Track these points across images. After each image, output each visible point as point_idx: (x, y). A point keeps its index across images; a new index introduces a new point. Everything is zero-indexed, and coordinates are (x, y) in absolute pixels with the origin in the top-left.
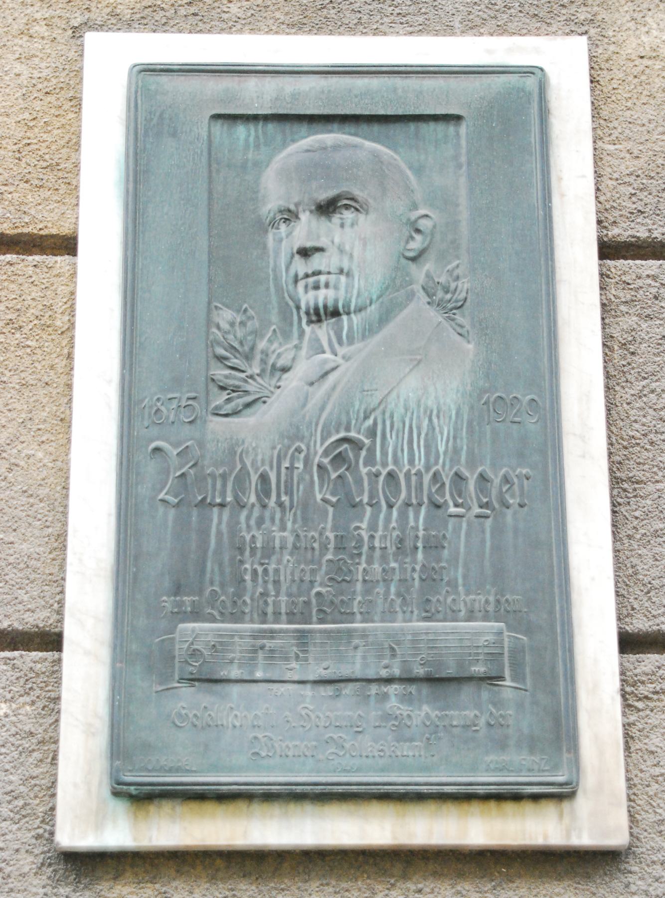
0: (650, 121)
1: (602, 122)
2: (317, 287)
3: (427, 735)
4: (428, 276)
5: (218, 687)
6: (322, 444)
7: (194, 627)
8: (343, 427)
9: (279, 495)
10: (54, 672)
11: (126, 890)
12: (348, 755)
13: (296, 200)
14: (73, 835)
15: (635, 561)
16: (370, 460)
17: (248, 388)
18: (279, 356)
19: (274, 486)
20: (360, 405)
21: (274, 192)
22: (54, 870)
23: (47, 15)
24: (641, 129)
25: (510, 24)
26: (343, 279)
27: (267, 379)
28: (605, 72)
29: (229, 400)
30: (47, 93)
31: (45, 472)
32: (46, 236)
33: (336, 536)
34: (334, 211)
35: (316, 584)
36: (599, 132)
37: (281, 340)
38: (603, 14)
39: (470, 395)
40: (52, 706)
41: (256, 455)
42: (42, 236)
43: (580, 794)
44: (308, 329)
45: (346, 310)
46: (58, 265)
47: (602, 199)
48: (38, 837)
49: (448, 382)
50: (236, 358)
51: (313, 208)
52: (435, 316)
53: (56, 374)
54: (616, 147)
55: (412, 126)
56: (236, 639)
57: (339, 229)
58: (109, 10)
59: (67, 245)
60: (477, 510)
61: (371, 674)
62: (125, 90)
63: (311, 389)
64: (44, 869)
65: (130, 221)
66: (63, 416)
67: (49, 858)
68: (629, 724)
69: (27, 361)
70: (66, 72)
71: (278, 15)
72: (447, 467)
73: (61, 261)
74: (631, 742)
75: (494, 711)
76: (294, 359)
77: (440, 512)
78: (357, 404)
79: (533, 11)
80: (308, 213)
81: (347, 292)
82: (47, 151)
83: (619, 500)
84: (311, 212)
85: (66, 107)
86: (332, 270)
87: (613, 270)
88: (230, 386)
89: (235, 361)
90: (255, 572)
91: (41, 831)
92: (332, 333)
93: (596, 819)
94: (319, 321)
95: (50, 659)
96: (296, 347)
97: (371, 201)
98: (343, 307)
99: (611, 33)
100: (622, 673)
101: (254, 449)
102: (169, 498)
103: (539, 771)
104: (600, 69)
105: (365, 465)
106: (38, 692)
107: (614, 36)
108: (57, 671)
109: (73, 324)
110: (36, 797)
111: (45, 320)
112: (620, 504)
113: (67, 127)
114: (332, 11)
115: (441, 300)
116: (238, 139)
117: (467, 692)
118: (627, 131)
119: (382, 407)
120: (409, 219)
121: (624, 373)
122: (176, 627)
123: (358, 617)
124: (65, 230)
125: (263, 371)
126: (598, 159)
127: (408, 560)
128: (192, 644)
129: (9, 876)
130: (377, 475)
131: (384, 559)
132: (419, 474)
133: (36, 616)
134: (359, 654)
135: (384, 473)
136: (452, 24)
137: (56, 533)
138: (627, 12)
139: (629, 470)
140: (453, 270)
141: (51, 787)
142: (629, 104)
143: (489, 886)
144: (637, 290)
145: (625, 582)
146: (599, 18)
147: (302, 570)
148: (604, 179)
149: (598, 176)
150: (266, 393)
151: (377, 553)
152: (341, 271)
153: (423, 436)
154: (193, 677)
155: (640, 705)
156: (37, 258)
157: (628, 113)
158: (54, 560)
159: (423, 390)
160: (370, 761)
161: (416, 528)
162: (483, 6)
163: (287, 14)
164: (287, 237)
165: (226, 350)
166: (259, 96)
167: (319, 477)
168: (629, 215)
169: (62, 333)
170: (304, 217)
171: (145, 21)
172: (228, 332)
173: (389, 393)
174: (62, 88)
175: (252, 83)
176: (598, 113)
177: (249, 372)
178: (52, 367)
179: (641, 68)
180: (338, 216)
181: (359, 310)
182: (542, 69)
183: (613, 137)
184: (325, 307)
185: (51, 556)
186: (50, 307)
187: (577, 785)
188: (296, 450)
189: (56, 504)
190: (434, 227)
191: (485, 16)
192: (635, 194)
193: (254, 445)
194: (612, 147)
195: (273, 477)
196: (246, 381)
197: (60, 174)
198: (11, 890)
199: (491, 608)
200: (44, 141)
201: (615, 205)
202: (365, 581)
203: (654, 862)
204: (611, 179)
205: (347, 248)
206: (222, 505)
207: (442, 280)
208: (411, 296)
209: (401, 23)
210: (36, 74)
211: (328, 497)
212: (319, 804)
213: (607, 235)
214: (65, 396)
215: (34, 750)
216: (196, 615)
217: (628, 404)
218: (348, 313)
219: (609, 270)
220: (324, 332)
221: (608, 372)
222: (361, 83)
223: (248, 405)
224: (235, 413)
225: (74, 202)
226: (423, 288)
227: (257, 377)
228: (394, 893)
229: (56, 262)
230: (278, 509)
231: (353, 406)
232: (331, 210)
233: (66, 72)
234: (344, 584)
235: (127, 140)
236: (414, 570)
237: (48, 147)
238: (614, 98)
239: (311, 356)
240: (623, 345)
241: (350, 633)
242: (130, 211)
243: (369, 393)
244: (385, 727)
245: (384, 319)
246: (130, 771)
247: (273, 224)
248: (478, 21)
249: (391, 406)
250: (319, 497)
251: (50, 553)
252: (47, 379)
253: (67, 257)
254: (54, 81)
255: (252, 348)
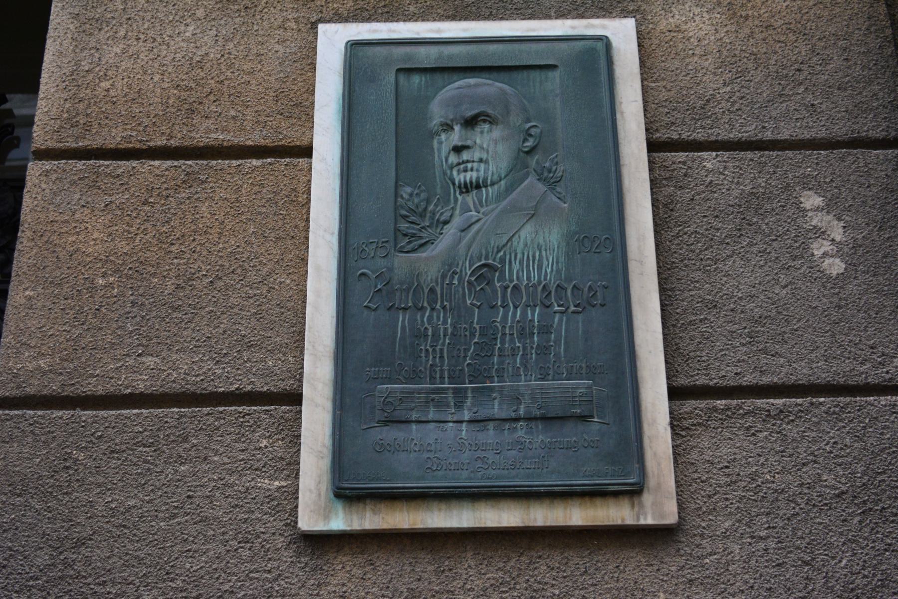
0: (677, 69)
2: (466, 171)
4: (537, 162)
9: (442, 302)
10: (297, 419)
13: (451, 117)
14: (307, 522)
15: (677, 341)
16: (502, 278)
17: (422, 235)
18: (442, 214)
19: (439, 296)
21: (437, 112)
26: (482, 165)
34: (476, 124)
38: (644, 7)
43: (645, 490)
44: (460, 198)
47: (648, 115)
48: (287, 525)
52: (541, 187)
57: (479, 135)
59: (307, 152)
60: (572, 308)
63: (463, 234)
65: (345, 134)
68: (676, 446)
69: (280, 223)
71: (439, 11)
74: (678, 457)
76: (451, 216)
77: (549, 309)
78: (492, 243)
79: (600, 5)
90: (427, 350)
91: (289, 521)
92: (475, 199)
94: (467, 192)
95: (295, 411)
96: (453, 208)
100: (671, 413)
105: (498, 282)
109: (310, 200)
110: (285, 499)
111: (293, 197)
117: (570, 425)
123: (496, 379)
125: (432, 224)
129: (268, 550)
130: (506, 288)
131: (512, 341)
132: (534, 286)
133: (285, 383)
135: (511, 286)
139: (672, 283)
143: (587, 553)
149: (645, 102)
152: (481, 161)
155: (683, 433)
156: (287, 160)
157: (663, 64)
159: (540, 244)
161: (532, 321)
166: (427, 56)
170: (457, 128)
175: (422, 50)
177: (423, 225)
178: (296, 227)
179: (670, 37)
181: (493, 184)
182: (607, 37)
186: (294, 190)
190: (541, 132)
194: (653, 85)
199: (584, 371)
202: (500, 356)
203: (695, 535)
205: (485, 146)
206: (405, 309)
207: (547, 165)
208: (527, 175)
210: (288, 51)
211: (475, 302)
212: (443, 506)
215: (284, 469)
218: (486, 186)
220: (470, 199)
222: (492, 47)
235: (344, 86)
236: (532, 348)
240: (665, 205)
241: (491, 389)
247: (438, 134)
249: (515, 243)
250: (469, 302)
252: (292, 234)
255: (425, 209)
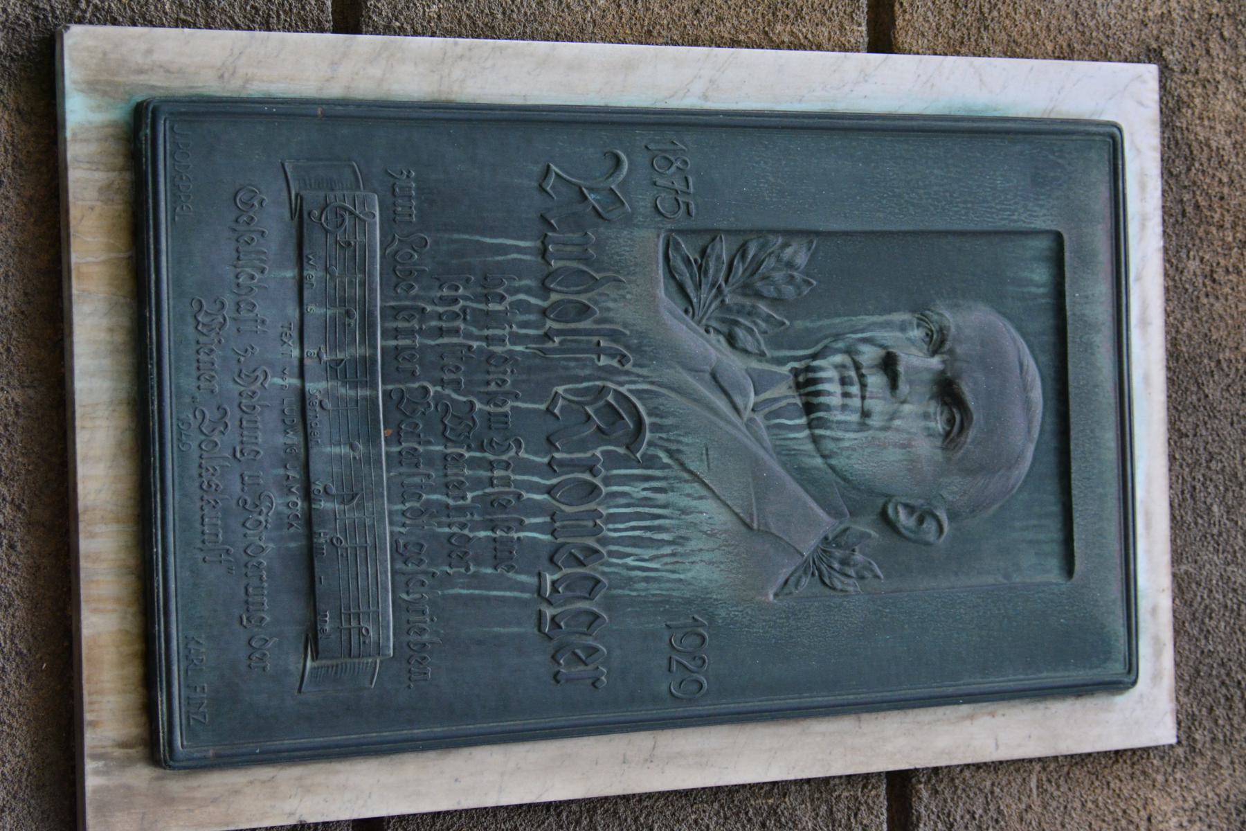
1: (1066, 769)
2: (844, 381)
3: (232, 550)
5: (291, 251)
6: (630, 391)
8: (657, 420)
9: (560, 332)
10: (305, 22)
12: (203, 437)
14: (80, 42)
16: (613, 460)
18: (750, 331)
19: (572, 326)
20: (687, 444)
21: (970, 320)
22: (28, 25)
23: (1174, 15)
24: (1058, 822)
25: (1186, 638)
26: (854, 418)
27: (716, 314)
28: (1130, 770)
29: (687, 261)
30: (1077, 14)
31: (578, 9)
32: (893, 11)
33: (506, 415)
34: (944, 403)
35: (439, 388)
36: (1052, 766)
37: (771, 332)
38: (1202, 764)
39: (703, 599)
40: (258, 19)
41: (615, 300)
42: (893, 6)
43: (158, 772)
44: (785, 370)
45: (815, 422)
46: (855, 27)
47: (967, 773)
49: (722, 566)
50: (745, 271)
51: (949, 374)
52: (809, 544)
53: (711, 24)
54: (1034, 791)
55: (1056, 509)
56: (359, 276)
57: (921, 410)
58: (1186, 99)
60: (549, 612)
61: (317, 466)
62: (1086, 117)
63: (707, 376)
64: (30, 11)
66: (655, 33)
67: (46, 18)
70: (1105, 41)
71: (1188, 324)
72: (607, 569)
73: (861, 31)
75: (270, 644)
76: (745, 351)
79: (1204, 670)
80: (941, 367)
81: (839, 422)
82: (1003, 13)
83: (564, 814)
84: (943, 372)
85: (1060, 39)
86: (868, 402)
87: (873, 793)
88: (707, 264)
89: (741, 270)
90: (455, 301)
94: (798, 386)
95: (323, 17)
96: (762, 354)
97: (960, 454)
98: (819, 419)
99: (1179, 775)
101: (624, 297)
102: (552, 179)
103: (188, 712)
104: (1133, 764)
105: (603, 453)
107: (1175, 780)
108: (307, 26)
109: (778, 48)
112: (559, 815)
113: (1035, 41)
114: (1194, 397)
116: (1032, 271)
118: (1054, 804)
119: (686, 476)
120: (936, 508)
121: (737, 815)
122: (375, 191)
123: (395, 449)
124: (903, 37)
125: (728, 309)
128: (351, 213)
130: (592, 470)
131: (477, 483)
132: (596, 530)
134: (345, 450)
135: (597, 481)
136: (1184, 560)
137: (496, 24)
138: (1206, 796)
140: (872, 570)
141: (144, 19)
142: (1090, 805)
145: (452, 826)
146: (1198, 760)
147: (458, 368)
148: (992, 775)
150: (699, 313)
151: (484, 474)
153: (648, 534)
154: (305, 216)
157: (1077, 804)
158: (460, 21)
160: (194, 472)
161: (521, 526)
162: (1207, 601)
163: (1190, 337)
164: (909, 339)
165: (753, 257)
166: (1089, 298)
167: (587, 388)
168: (946, 811)
169: (766, 33)
170: (935, 362)
171: (1172, 146)
172: (779, 259)
173: (706, 485)
174: (1083, 33)
175: (1102, 288)
176: (1077, 763)
177: (726, 290)
178: (720, 19)
179: (1136, 819)
180: (939, 410)
181: (815, 440)
182: (1134, 683)
183: (1047, 785)
185: (464, 18)
186: (799, 15)
187: (171, 767)
188: (624, 356)
189: (536, 25)
190: (927, 544)
191: (1196, 605)
192: (974, 818)
193: (628, 296)
194: (1033, 784)
196: (713, 285)
197: (974, 31)
199: (413, 637)
200: (1015, 10)
201: (959, 792)
202: (445, 457)
204: (993, 784)
205: (897, 422)
207: (858, 557)
208: (834, 512)
209: (1183, 492)
211: (560, 402)
213: (920, 782)
214: (682, 37)
216: (390, 220)
217: (696, 821)
218: (810, 425)
219: (873, 787)
221: (738, 791)
222: (1110, 437)
223: (681, 288)
224: (670, 271)
225: (939, 49)
226: (845, 530)
227: (719, 300)
229: (860, 25)
230: (540, 332)
231: (686, 434)
232: (947, 399)
233: (1105, 41)
234: (441, 427)
236: (463, 526)
237: (1008, 14)
238: (1097, 783)
239: (751, 377)
241: (373, 439)
242: (934, 123)
243: (704, 457)
244: (243, 490)
245: (803, 476)
246: (172, 128)
248: (1188, 596)
250: (560, 389)
251: (468, 16)
252: (704, 11)
253: (867, 39)
254: (1092, 24)
255: (759, 295)
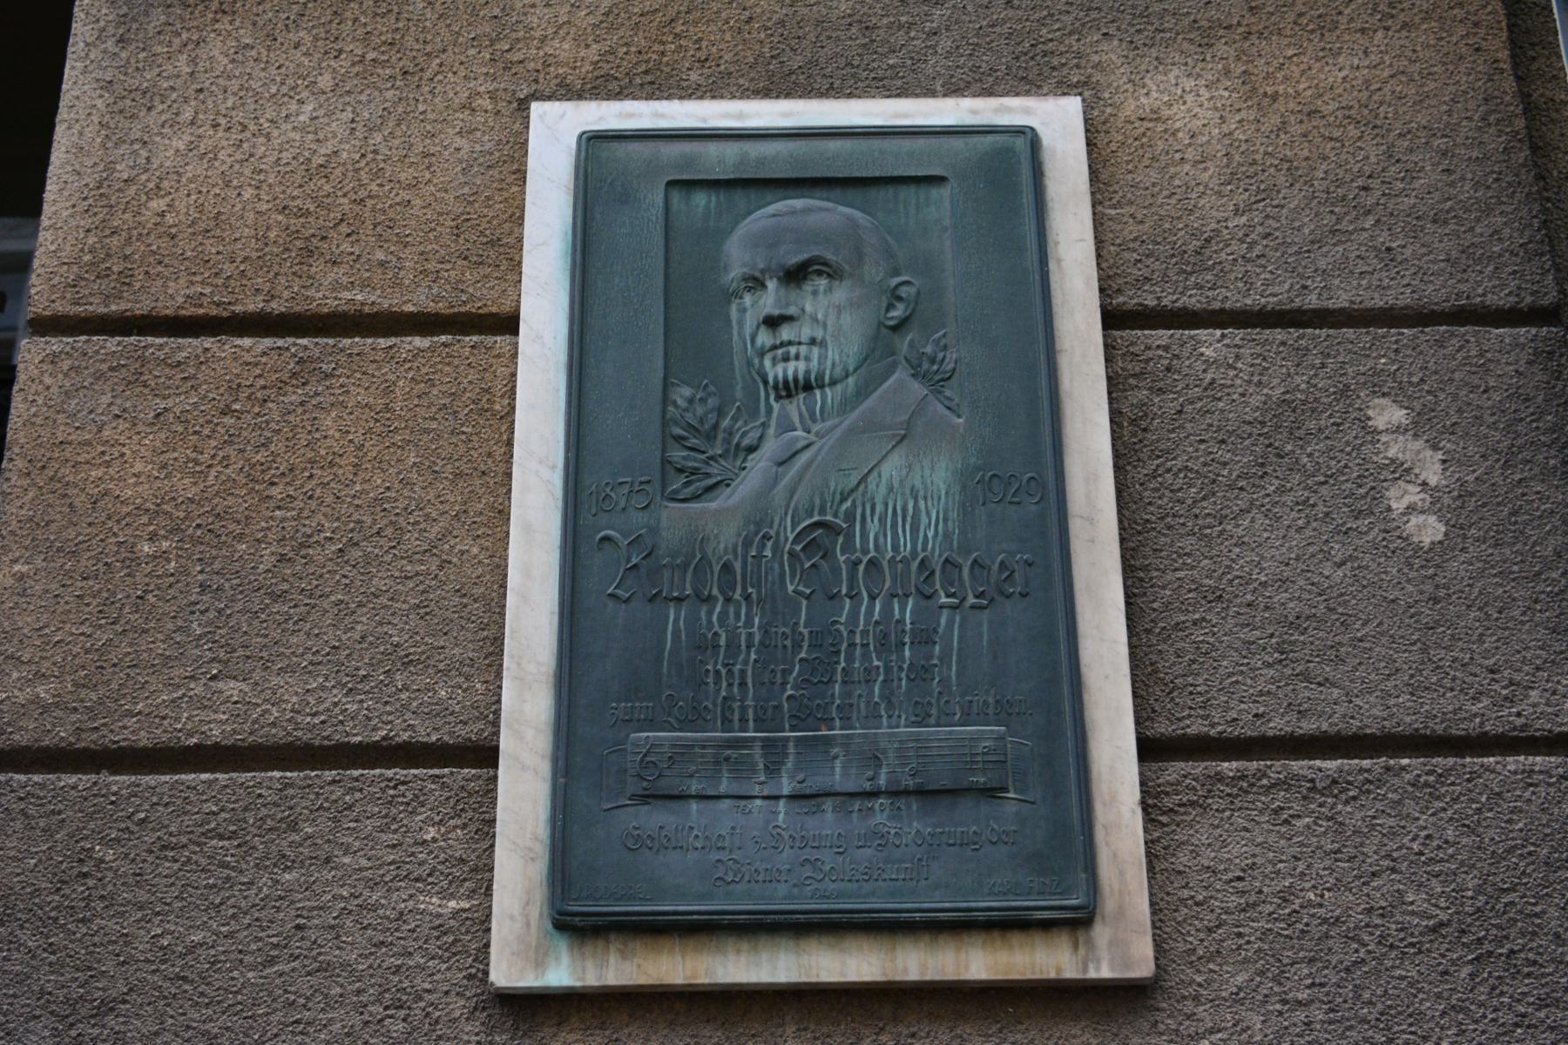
0: (1154, 185)
2: (786, 359)
4: (911, 345)
7: (654, 746)
9: (744, 588)
11: (571, 1037)
13: (762, 266)
15: (1154, 657)
16: (848, 547)
18: (744, 434)
19: (739, 577)
21: (737, 256)
26: (816, 351)
34: (805, 278)
43: (1098, 919)
44: (776, 406)
47: (1104, 265)
48: (470, 977)
52: (918, 389)
57: (810, 297)
59: (509, 324)
60: (971, 600)
61: (851, 786)
68: (1152, 841)
69: (462, 449)
71: (741, 81)
73: (500, 340)
76: (761, 438)
77: (930, 603)
79: (1021, 73)
84: (779, 278)
90: (717, 672)
91: (473, 971)
93: (1121, 949)
94: (789, 396)
95: (485, 777)
96: (763, 424)
99: (1107, 95)
106: (470, 814)
109: (514, 408)
110: (467, 932)
111: (484, 404)
115: (927, 372)
119: (861, 488)
123: (838, 723)
124: (506, 307)
125: (727, 451)
126: (1098, 222)
127: (894, 657)
129: (437, 1022)
130: (856, 563)
131: (866, 656)
132: (904, 560)
133: (468, 729)
135: (865, 560)
143: (994, 1029)
144: (1148, 361)
150: (730, 475)
155: (1164, 819)
156: (475, 338)
157: (1130, 177)
161: (901, 622)
163: (752, 80)
166: (721, 160)
170: (771, 285)
177: (711, 453)
178: (490, 455)
181: (833, 383)
182: (1032, 129)
184: (796, 380)
186: (487, 391)
190: (918, 293)
194: (1113, 212)
195: (738, 566)
198: (440, 1037)
199: (991, 711)
203: (1184, 998)
205: (820, 316)
207: (929, 349)
210: (478, 148)
211: (801, 588)
215: (465, 880)
216: (651, 724)
218: (822, 387)
220: (794, 408)
222: (833, 145)
223: (709, 489)
224: (695, 498)
228: (883, 1038)
231: (828, 487)
236: (901, 668)
240: (1133, 422)
241: (828, 741)
245: (863, 392)
248: (962, 85)
249: (872, 487)
254: (497, 154)
255: (716, 426)
